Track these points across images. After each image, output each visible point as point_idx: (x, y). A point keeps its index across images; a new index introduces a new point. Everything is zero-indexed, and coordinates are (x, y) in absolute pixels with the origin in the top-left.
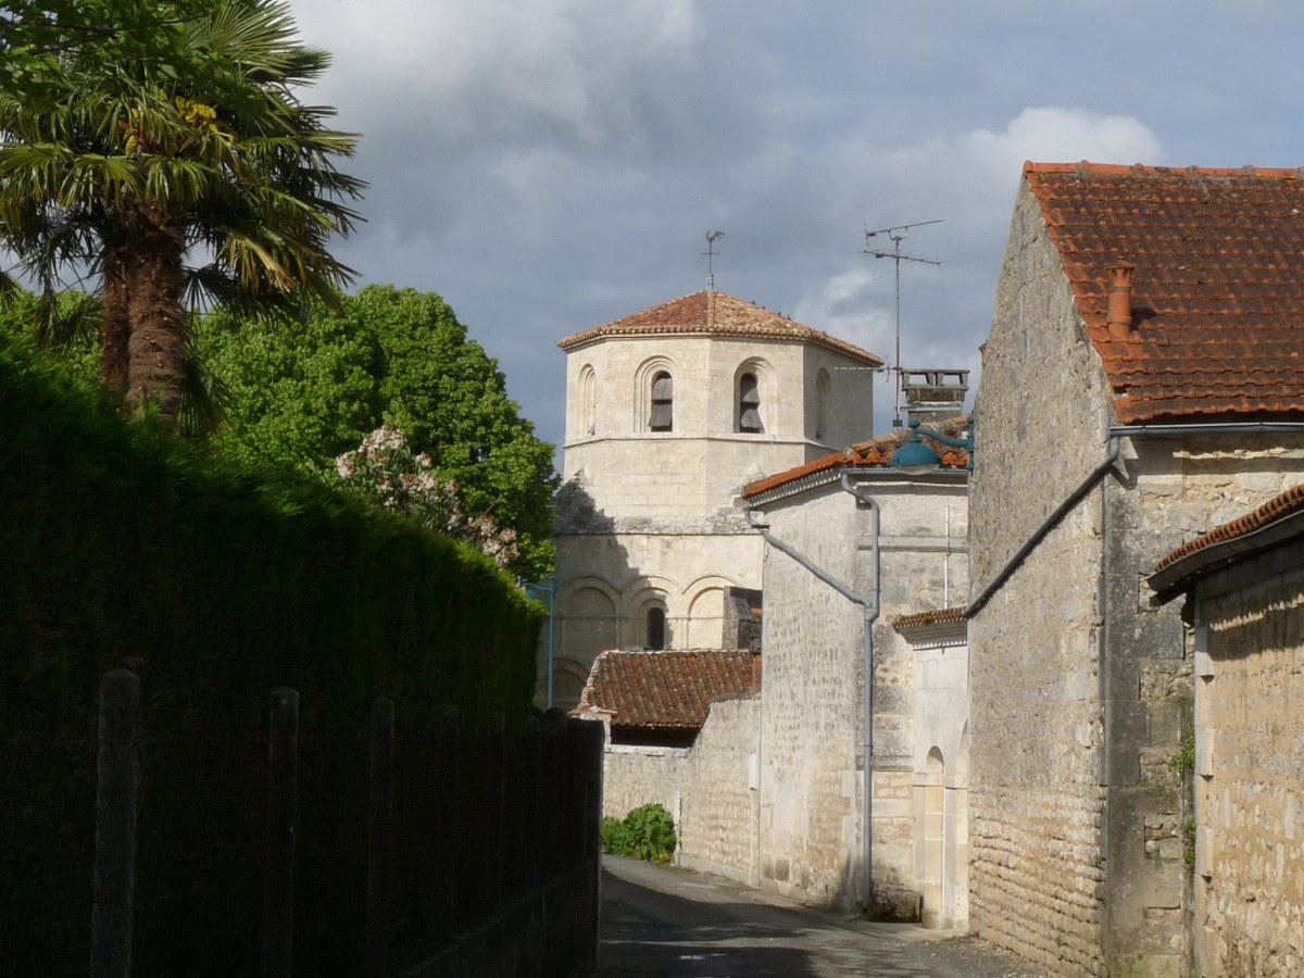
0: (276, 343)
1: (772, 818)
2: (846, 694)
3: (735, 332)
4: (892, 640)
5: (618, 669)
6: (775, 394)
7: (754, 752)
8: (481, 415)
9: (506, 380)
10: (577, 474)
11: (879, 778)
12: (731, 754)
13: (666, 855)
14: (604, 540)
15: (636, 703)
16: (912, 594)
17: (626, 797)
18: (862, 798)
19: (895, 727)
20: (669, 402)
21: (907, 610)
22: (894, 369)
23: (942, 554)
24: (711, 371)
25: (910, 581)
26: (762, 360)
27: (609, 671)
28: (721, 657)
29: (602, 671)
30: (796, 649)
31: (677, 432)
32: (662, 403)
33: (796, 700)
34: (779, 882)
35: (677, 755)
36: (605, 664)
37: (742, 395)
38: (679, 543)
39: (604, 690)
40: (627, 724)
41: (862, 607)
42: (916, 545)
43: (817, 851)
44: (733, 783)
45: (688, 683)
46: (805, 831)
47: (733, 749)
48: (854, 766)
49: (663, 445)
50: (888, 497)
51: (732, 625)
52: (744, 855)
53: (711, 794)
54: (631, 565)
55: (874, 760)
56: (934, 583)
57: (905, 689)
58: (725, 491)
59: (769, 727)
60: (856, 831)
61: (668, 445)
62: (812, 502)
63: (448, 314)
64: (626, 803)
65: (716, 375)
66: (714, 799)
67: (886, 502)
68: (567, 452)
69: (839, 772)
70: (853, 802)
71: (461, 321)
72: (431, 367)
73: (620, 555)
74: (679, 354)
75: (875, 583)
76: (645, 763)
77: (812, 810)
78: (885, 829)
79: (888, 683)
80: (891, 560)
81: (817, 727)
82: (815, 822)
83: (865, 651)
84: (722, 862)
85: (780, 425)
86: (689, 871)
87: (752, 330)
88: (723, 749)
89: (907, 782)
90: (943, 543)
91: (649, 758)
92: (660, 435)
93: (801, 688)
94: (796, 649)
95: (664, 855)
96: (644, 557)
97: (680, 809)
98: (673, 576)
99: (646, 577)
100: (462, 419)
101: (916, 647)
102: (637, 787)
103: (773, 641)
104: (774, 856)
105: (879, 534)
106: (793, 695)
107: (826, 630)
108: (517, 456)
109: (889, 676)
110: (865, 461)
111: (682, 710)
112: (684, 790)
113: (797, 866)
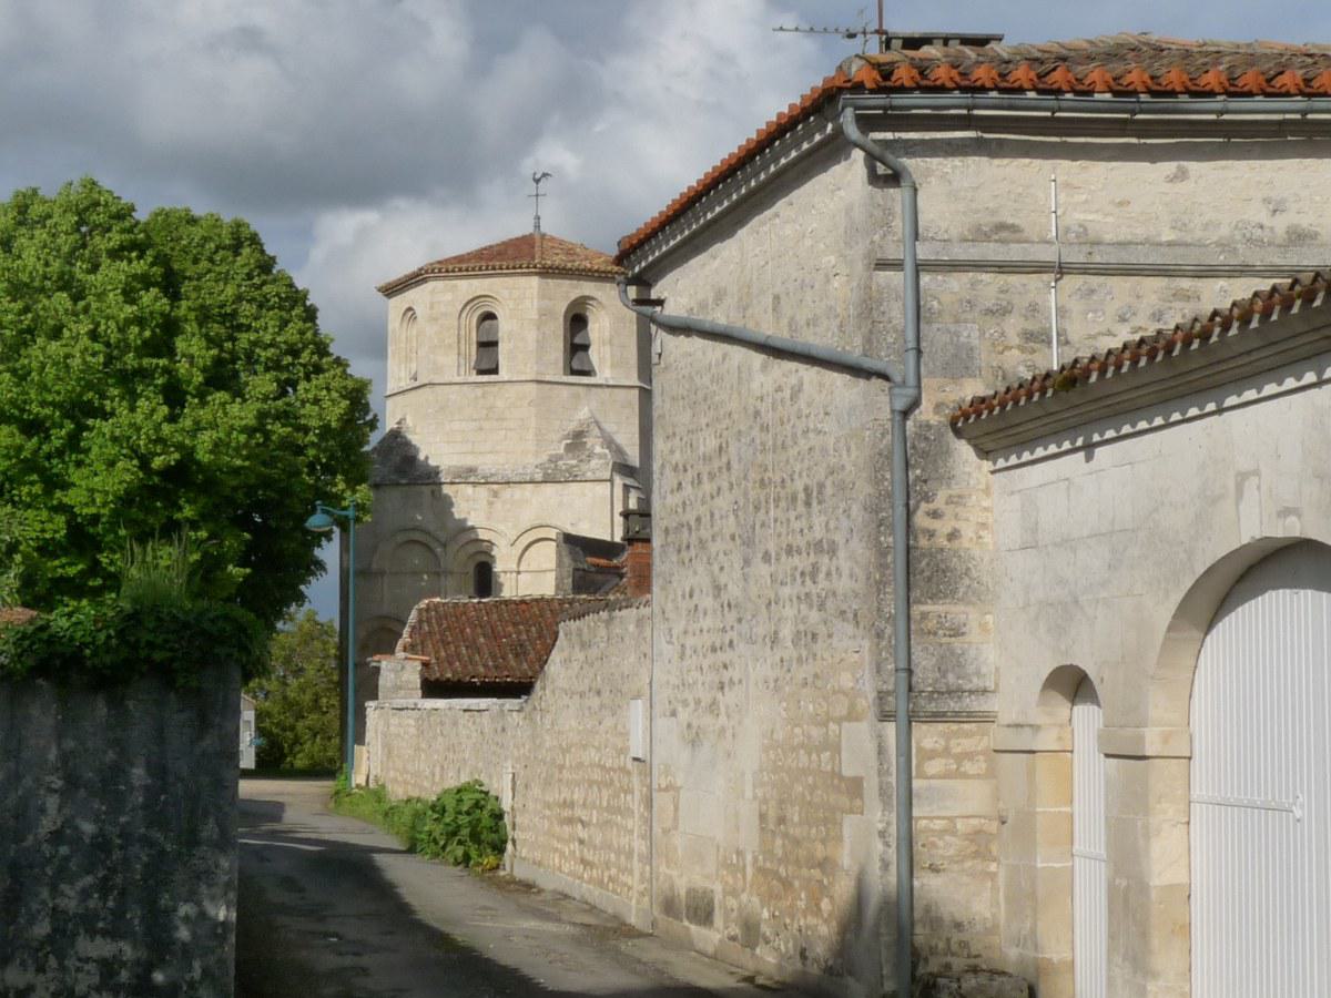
0: (51, 258)
1: (676, 809)
2: (850, 567)
3: (564, 269)
4: (948, 452)
5: (439, 619)
6: (607, 334)
7: (637, 697)
8: (285, 342)
9: (319, 314)
10: (399, 423)
11: (927, 736)
12: (595, 702)
13: (492, 858)
14: (426, 490)
15: (458, 655)
16: (984, 357)
17: (438, 770)
18: (893, 779)
19: (957, 632)
20: (494, 344)
21: (972, 389)
22: (877, 32)
23: (1045, 277)
24: (539, 310)
25: (982, 333)
26: (593, 299)
27: (429, 621)
28: (556, 604)
29: (420, 621)
30: (723, 503)
31: (503, 374)
32: (488, 345)
33: (725, 597)
34: (693, 928)
35: (507, 707)
36: (424, 614)
37: (573, 336)
38: (507, 492)
39: (422, 643)
40: (448, 680)
41: (886, 385)
42: (992, 257)
43: (780, 879)
44: (598, 749)
45: (519, 633)
46: (749, 839)
47: (599, 693)
48: (871, 714)
49: (488, 389)
50: (934, 162)
51: (565, 574)
52: (623, 871)
53: (561, 768)
54: (457, 516)
55: (917, 697)
56: (1029, 336)
57: (976, 552)
58: (555, 437)
59: (668, 650)
60: (880, 846)
61: (495, 389)
62: (756, 220)
63: (254, 240)
64: (437, 778)
65: (544, 314)
66: (566, 774)
67: (928, 173)
68: (390, 403)
69: (833, 727)
70: (871, 786)
71: (270, 250)
72: (230, 291)
73: (447, 503)
74: (506, 293)
75: (911, 335)
76: (461, 721)
77: (765, 801)
78: (941, 843)
79: (942, 542)
80: (944, 290)
81: (775, 639)
82: (772, 823)
83: (893, 477)
84: (581, 878)
85: (613, 366)
86: (528, 887)
87: (582, 267)
88: (582, 695)
89: (984, 743)
90: (1047, 254)
91: (636, 763)
92: (485, 378)
93: (737, 574)
94: (723, 503)
95: (490, 860)
96: (469, 506)
97: (513, 789)
98: (501, 527)
99: (473, 528)
100: (266, 347)
101: (1001, 463)
102: (451, 756)
103: (673, 500)
104: (684, 879)
105: (916, 236)
106: (718, 589)
107: (793, 452)
108: (328, 389)
109: (942, 527)
110: (888, 84)
111: (513, 663)
112: (518, 760)
113: (732, 902)
